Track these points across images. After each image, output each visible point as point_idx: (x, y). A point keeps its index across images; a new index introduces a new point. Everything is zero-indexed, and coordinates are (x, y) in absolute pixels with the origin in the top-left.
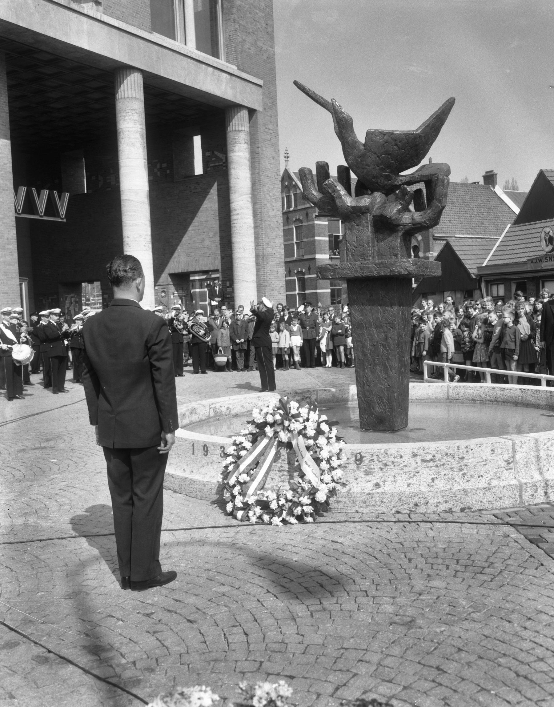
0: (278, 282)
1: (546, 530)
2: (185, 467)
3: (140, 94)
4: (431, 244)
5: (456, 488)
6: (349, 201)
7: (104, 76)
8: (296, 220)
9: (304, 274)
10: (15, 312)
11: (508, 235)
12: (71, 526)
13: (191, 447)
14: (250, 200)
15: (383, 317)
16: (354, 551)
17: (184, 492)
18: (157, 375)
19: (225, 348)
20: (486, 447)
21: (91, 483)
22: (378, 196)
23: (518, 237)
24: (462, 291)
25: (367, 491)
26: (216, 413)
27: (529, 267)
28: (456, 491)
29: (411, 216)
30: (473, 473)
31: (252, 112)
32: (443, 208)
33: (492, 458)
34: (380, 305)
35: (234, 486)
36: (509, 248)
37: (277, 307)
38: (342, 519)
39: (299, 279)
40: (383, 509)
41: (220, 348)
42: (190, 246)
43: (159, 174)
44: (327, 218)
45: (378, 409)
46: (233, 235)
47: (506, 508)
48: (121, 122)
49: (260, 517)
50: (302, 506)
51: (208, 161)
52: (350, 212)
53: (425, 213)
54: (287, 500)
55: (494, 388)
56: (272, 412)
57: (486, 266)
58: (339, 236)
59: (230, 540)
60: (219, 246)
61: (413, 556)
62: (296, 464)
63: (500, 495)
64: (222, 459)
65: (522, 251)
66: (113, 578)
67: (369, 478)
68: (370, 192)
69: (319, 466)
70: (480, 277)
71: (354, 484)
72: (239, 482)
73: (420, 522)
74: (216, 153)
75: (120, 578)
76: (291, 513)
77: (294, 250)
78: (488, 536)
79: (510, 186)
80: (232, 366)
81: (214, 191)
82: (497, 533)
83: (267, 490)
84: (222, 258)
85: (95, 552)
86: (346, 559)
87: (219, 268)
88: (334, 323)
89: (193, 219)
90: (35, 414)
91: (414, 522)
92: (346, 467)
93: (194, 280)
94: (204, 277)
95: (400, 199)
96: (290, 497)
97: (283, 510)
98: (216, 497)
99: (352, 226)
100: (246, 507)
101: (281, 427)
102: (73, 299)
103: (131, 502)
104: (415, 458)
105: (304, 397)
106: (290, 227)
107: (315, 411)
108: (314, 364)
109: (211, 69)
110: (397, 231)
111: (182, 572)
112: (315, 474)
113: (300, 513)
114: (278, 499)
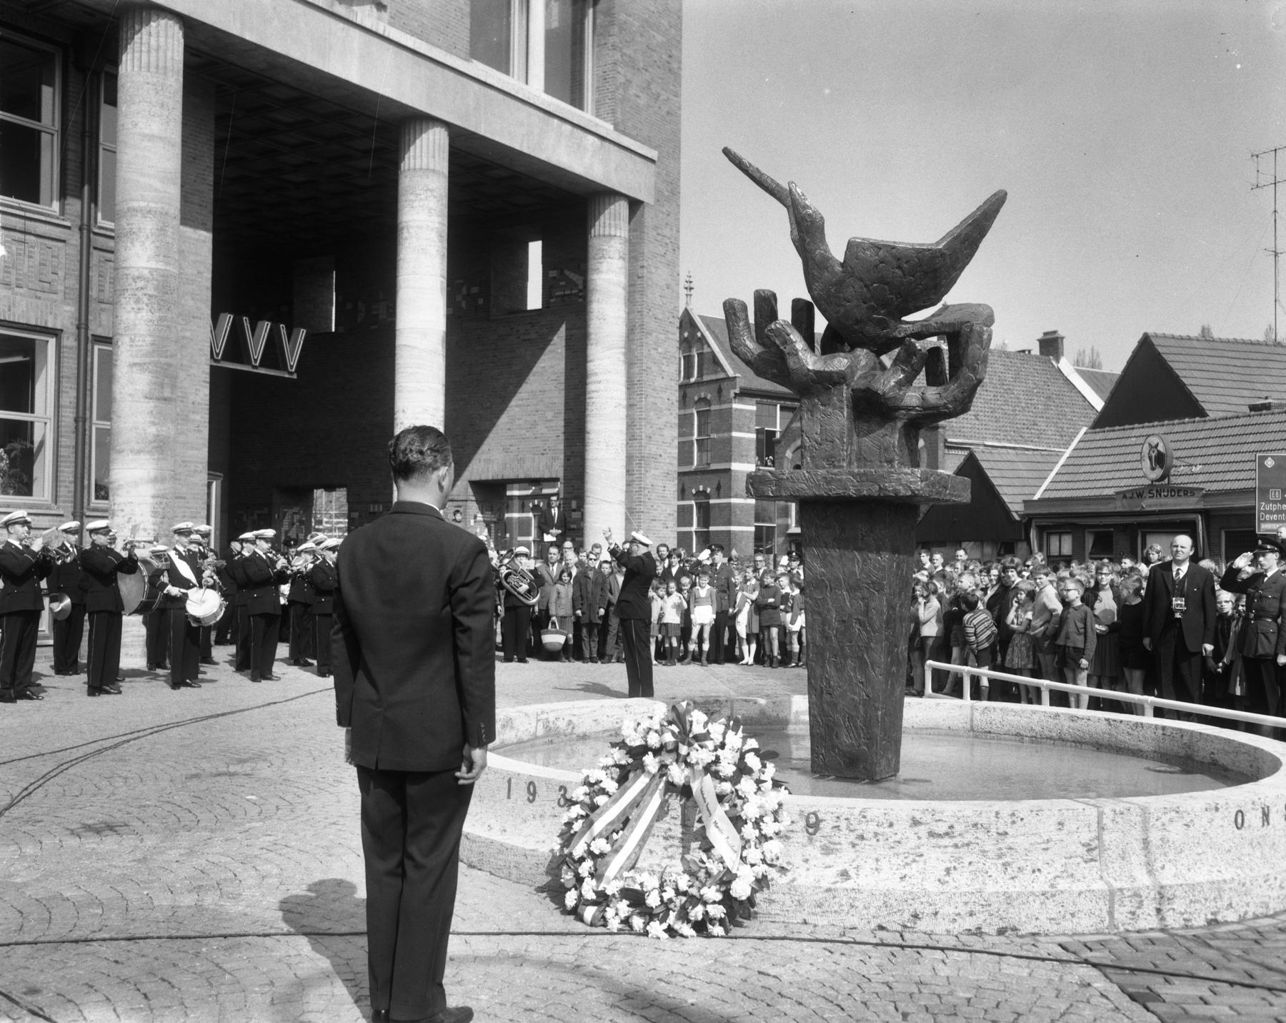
0: (664, 507)
1: (1160, 979)
2: (492, 822)
3: (443, 165)
4: (940, 459)
5: (990, 888)
6: (811, 361)
7: (389, 127)
8: (700, 399)
9: (708, 496)
10: (197, 532)
11: (1082, 445)
12: (280, 914)
13: (506, 785)
14: (622, 358)
15: (862, 570)
16: (800, 992)
17: (485, 867)
18: (463, 641)
19: (562, 619)
20: (1049, 817)
21: (327, 838)
22: (863, 355)
23: (1099, 452)
24: (993, 542)
25: (825, 885)
26: (547, 728)
27: (1119, 506)
28: (991, 894)
29: (919, 393)
30: (1022, 864)
31: (635, 205)
32: (980, 381)
34: (859, 550)
35: (582, 860)
37: (658, 551)
38: (778, 934)
39: (699, 506)
40: (854, 921)
41: (554, 618)
42: (510, 433)
43: (464, 305)
44: (754, 400)
45: (846, 740)
46: (589, 419)
48: (406, 210)
49: (626, 921)
50: (705, 903)
51: (551, 287)
52: (813, 381)
53: (946, 390)
54: (678, 892)
55: (1057, 715)
56: (657, 727)
57: (1040, 500)
58: (774, 432)
59: (571, 959)
60: (562, 437)
61: (911, 1008)
62: (697, 826)
63: (1072, 909)
64: (560, 809)
65: (1107, 475)
66: (356, 1012)
67: (829, 860)
68: (847, 348)
69: (739, 832)
70: (1028, 520)
71: (802, 871)
72: (591, 854)
73: (923, 947)
74: (567, 273)
75: (370, 1011)
76: (683, 916)
77: (692, 452)
78: (1050, 981)
79: (1087, 360)
80: (572, 652)
81: (558, 343)
82: (1068, 978)
83: (641, 871)
84: (567, 458)
85: (325, 963)
86: (786, 1006)
87: (561, 475)
88: (764, 587)
89: (519, 385)
90: (218, 715)
91: (911, 947)
92: (787, 837)
93: (512, 497)
94: (529, 492)
95: (903, 363)
96: (683, 886)
97: (668, 909)
98: (546, 879)
99: (814, 406)
100: (603, 899)
101: (674, 755)
102: (296, 517)
103: (400, 871)
104: (916, 829)
105: (711, 708)
106: (688, 411)
107: (736, 730)
108: (722, 657)
109: (568, 127)
110: (894, 419)
111: (482, 1011)
112: (732, 847)
113: (700, 917)
114: (662, 888)
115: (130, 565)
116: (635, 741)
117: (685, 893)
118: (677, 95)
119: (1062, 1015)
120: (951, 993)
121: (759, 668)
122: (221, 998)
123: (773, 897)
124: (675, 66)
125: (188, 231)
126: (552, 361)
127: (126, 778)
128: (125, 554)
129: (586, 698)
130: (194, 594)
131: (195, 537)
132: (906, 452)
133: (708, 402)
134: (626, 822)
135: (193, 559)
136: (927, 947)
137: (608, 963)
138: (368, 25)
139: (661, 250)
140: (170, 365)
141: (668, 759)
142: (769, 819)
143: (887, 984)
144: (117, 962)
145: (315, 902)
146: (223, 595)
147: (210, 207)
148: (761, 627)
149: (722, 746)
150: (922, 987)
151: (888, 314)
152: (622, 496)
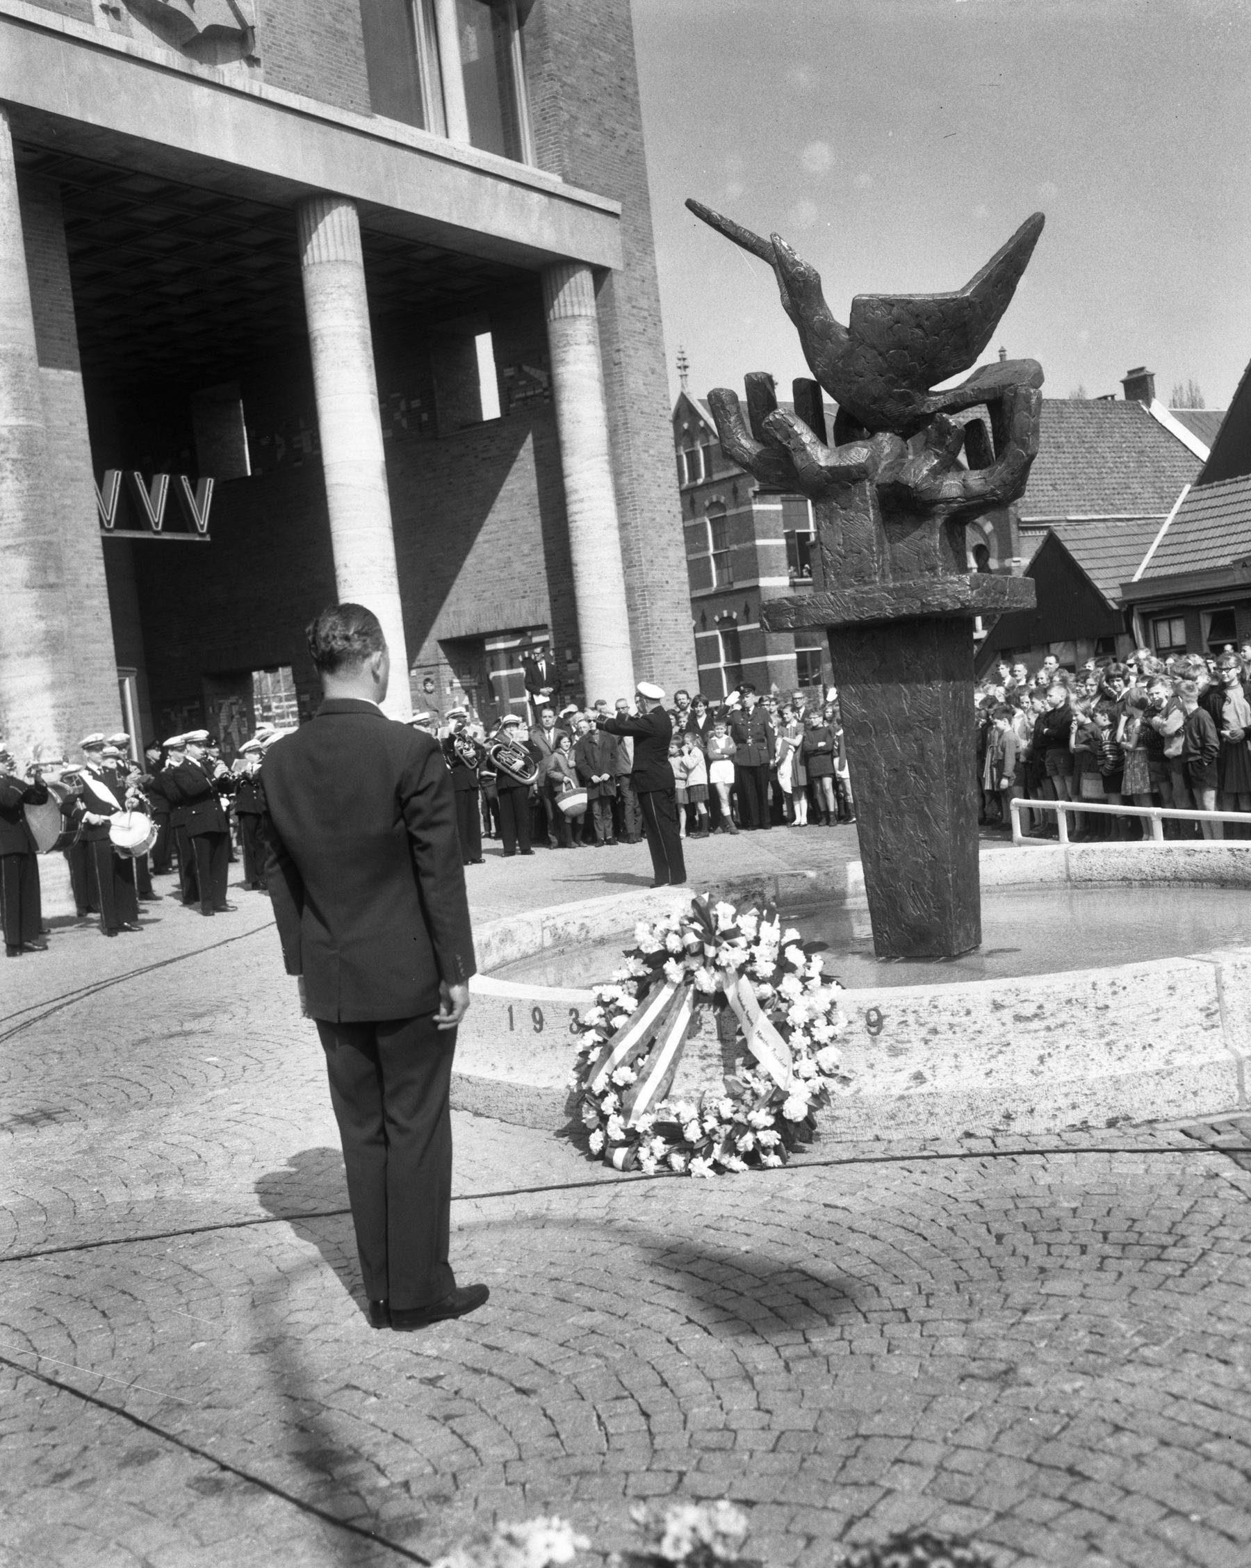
0: (678, 645)
3: (355, 253)
5: (1093, 1074)
6: (823, 456)
7: (283, 213)
9: (735, 623)
10: (112, 743)
11: (1186, 508)
12: (256, 1197)
14: (606, 467)
15: (911, 707)
17: (495, 1114)
18: (424, 859)
22: (886, 442)
24: (1089, 639)
25: (896, 1092)
30: (1130, 1040)
31: (600, 274)
33: (1172, 1004)
34: (904, 681)
35: (604, 1094)
36: (1191, 537)
40: (931, 1132)
43: (404, 423)
44: (779, 498)
45: (913, 911)
47: (1210, 1115)
49: (664, 1161)
50: (755, 1130)
51: (510, 389)
52: (827, 480)
53: (991, 473)
54: (721, 1121)
55: (1170, 851)
56: (677, 927)
57: (1141, 581)
58: (808, 534)
59: (602, 1213)
60: (544, 573)
61: (1005, 1228)
63: (1194, 1087)
65: (1220, 542)
66: (353, 1305)
67: (899, 1061)
69: (787, 1041)
70: (1128, 608)
71: (867, 1078)
72: (614, 1086)
73: (1019, 1153)
74: (526, 368)
75: (367, 1304)
76: (730, 1147)
77: (710, 571)
78: (1170, 1177)
79: (1185, 399)
83: (675, 1099)
84: (554, 599)
85: (312, 1250)
86: (856, 1242)
87: (548, 620)
89: (484, 516)
90: (166, 963)
94: (517, 643)
95: (935, 445)
96: (726, 1113)
97: (712, 1142)
98: (567, 1121)
99: (832, 510)
100: (633, 1139)
101: (700, 959)
102: (235, 709)
103: (382, 1137)
104: (998, 1014)
106: (698, 521)
107: (770, 920)
108: (768, 820)
109: (504, 186)
111: (499, 1287)
113: (750, 1147)
114: (701, 1118)
115: (38, 794)
116: (651, 946)
117: (730, 1121)
118: (637, 127)
119: (1185, 1215)
120: (1053, 1205)
121: (815, 828)
122: (193, 1306)
123: (837, 1113)
124: (630, 90)
125: (52, 374)
126: (521, 481)
127: (61, 1053)
128: (30, 782)
129: (606, 892)
130: (117, 819)
131: (113, 750)
132: (951, 554)
133: (723, 507)
134: (651, 1044)
135: (111, 778)
136: (1025, 1152)
137: (645, 1213)
138: (239, 86)
139: (639, 326)
140: (50, 543)
141: (694, 964)
142: (821, 1022)
143: (977, 1202)
144: (67, 1277)
145: (296, 1178)
146: (153, 818)
147: (74, 340)
148: (809, 778)
149: (757, 941)
150: (1018, 1201)
151: (912, 386)
152: (625, 638)
